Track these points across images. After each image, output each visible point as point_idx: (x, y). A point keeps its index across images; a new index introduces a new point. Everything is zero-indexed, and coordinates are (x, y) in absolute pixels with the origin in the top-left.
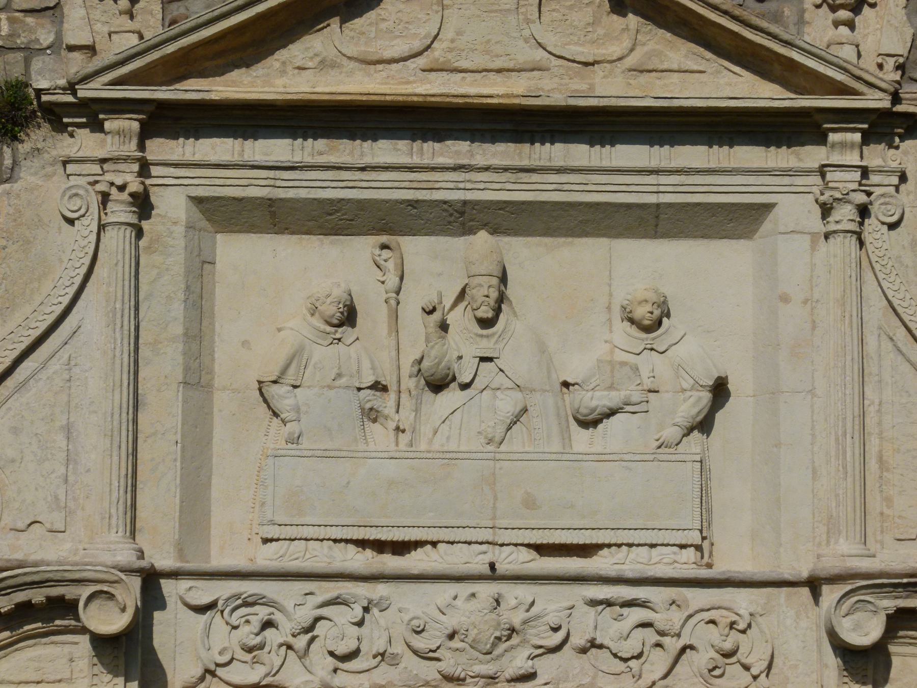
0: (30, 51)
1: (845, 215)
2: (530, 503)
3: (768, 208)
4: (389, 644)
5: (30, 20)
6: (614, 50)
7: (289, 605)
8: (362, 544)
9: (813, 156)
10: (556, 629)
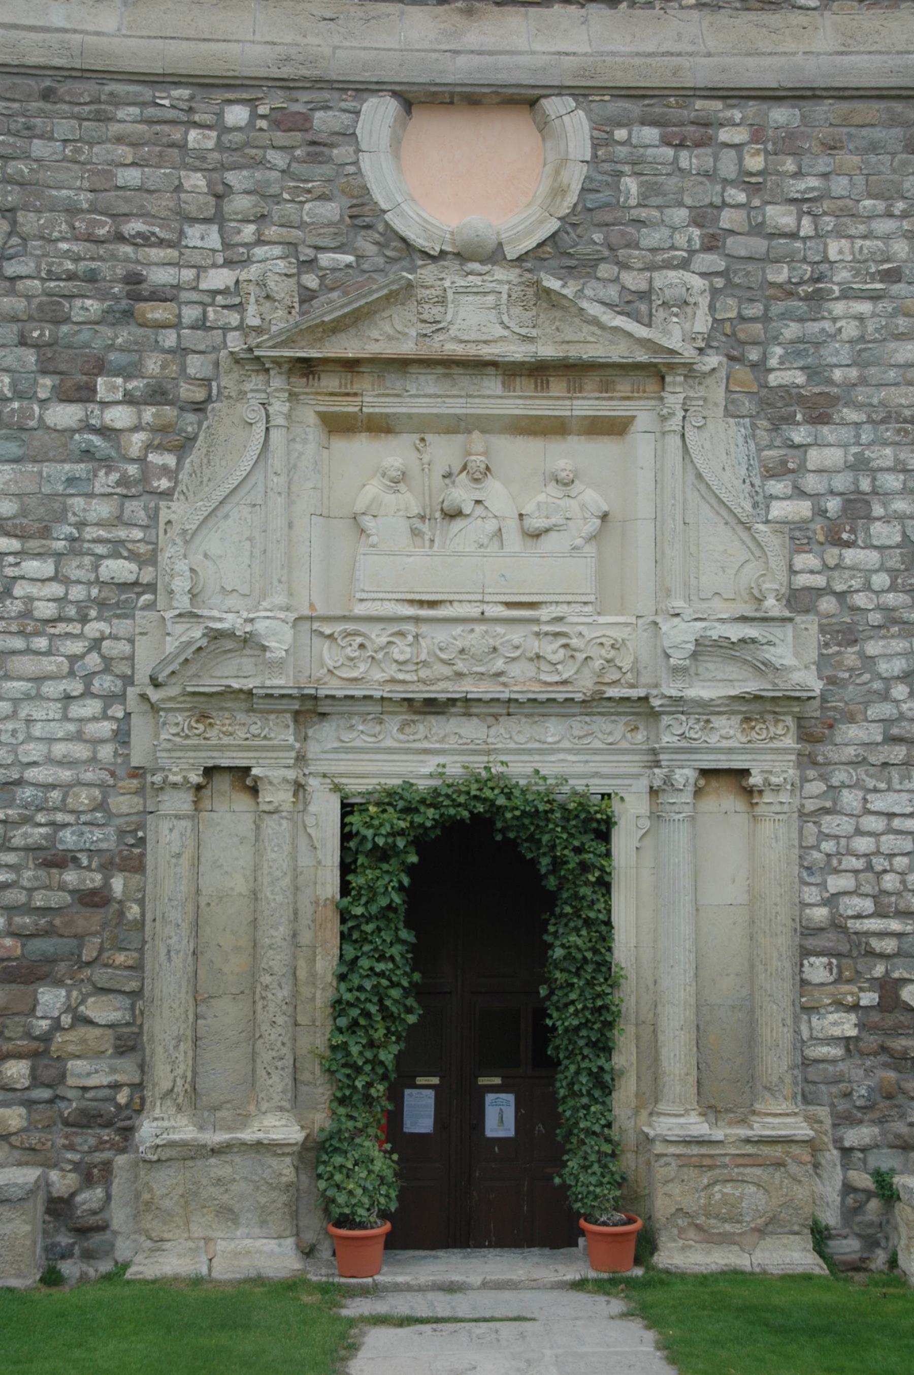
3: (635, 417)
5: (225, 311)
7: (373, 636)
8: (411, 602)
10: (517, 647)
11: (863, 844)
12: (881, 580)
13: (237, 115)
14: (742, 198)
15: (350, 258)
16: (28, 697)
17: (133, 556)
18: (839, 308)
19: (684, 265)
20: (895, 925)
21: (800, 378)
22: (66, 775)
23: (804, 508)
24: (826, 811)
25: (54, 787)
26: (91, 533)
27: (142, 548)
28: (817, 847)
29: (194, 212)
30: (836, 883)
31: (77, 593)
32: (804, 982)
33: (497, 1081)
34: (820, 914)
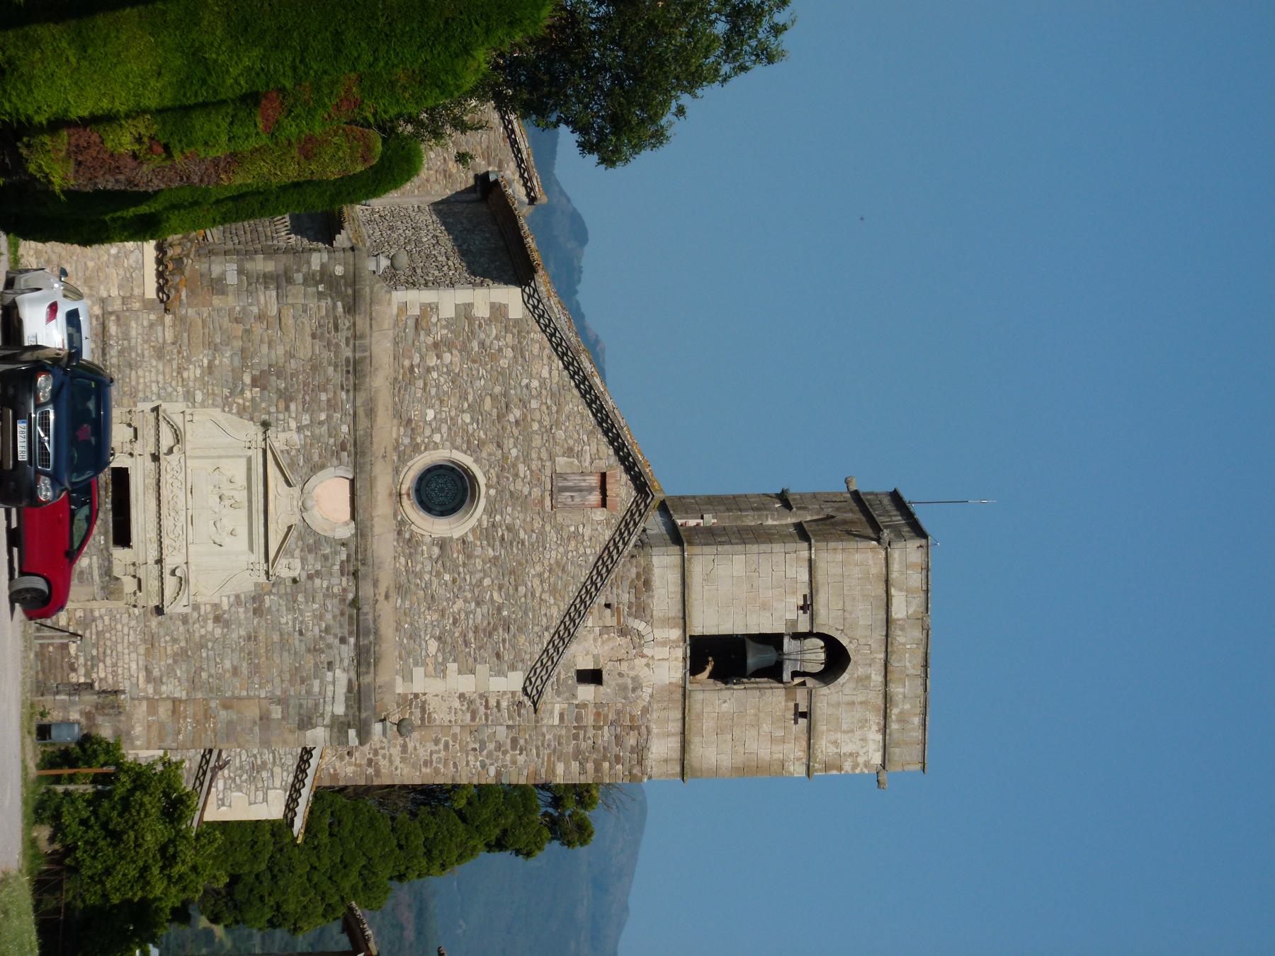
0: (277, 427)
1: (251, 567)
2: (200, 515)
4: (399, 505)
6: (280, 526)
9: (263, 561)
11: (119, 627)
12: (203, 632)
13: (345, 428)
14: (325, 586)
15: (301, 465)
16: (158, 370)
17: (203, 401)
18: (290, 617)
19: (303, 568)
20: (94, 637)
21: (266, 606)
22: (133, 383)
23: (226, 607)
24: (129, 616)
25: (130, 379)
26: (210, 388)
27: (206, 403)
28: (118, 613)
29: (314, 416)
30: (107, 619)
31: (191, 384)
32: (76, 610)
33: (14, 525)
34: (97, 614)
